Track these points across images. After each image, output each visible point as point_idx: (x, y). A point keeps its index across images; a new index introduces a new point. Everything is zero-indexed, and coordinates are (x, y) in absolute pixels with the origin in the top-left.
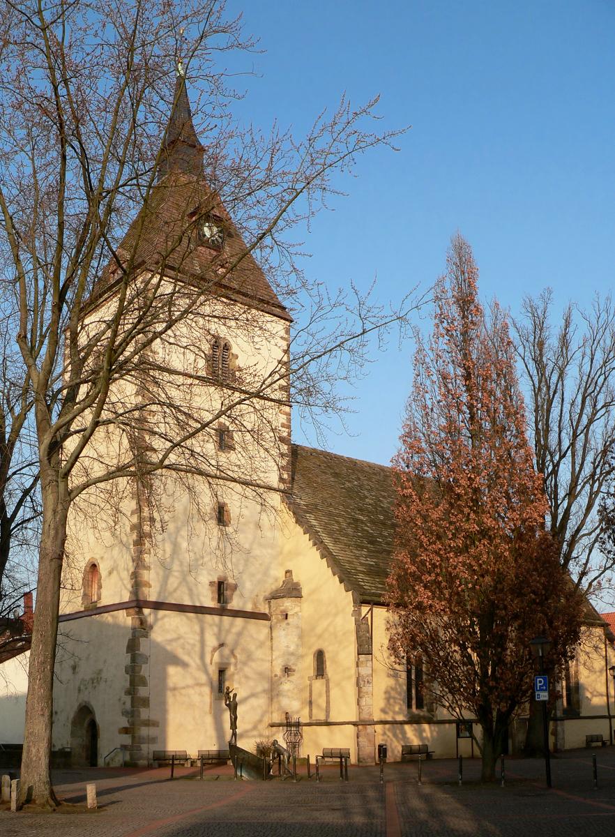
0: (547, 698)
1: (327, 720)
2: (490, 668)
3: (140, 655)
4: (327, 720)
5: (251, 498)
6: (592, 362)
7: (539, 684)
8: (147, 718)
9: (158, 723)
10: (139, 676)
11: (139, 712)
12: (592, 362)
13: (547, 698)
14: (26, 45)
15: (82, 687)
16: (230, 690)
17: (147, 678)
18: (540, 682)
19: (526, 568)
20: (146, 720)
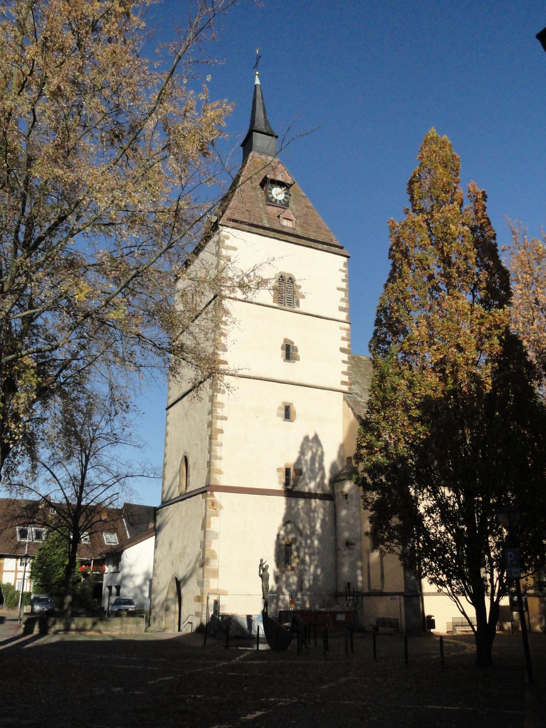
0: (344, 619)
1: (382, 590)
2: (125, 525)
3: (210, 531)
4: (382, 590)
5: (98, 373)
6: (173, 70)
7: (509, 559)
8: (216, 587)
9: (227, 592)
10: (210, 550)
11: (208, 582)
12: (173, 70)
13: (344, 619)
14: (145, 271)
15: (174, 561)
16: (263, 562)
17: (217, 551)
18: (511, 556)
19: (416, 413)
20: (215, 590)
